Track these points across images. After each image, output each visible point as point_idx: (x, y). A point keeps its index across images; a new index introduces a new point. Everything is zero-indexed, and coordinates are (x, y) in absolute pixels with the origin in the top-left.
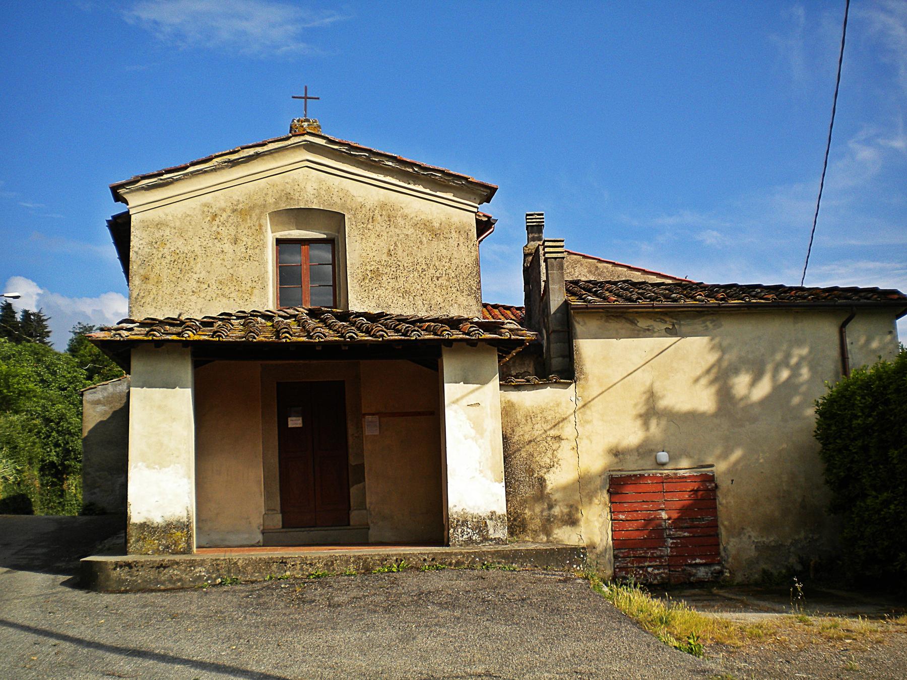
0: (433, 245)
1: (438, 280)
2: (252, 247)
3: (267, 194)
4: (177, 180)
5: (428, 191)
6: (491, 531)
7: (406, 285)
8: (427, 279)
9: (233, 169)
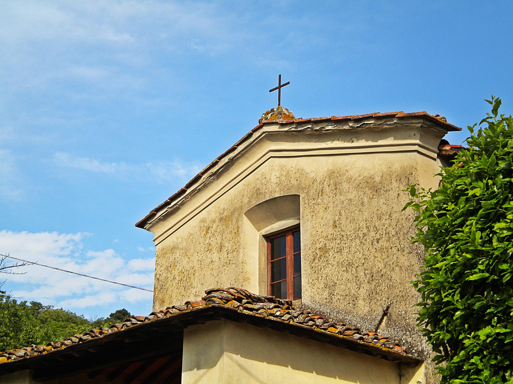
0: (373, 203)
1: (378, 242)
2: (231, 251)
4: (183, 204)
7: (349, 256)
8: (368, 245)
9: (219, 180)
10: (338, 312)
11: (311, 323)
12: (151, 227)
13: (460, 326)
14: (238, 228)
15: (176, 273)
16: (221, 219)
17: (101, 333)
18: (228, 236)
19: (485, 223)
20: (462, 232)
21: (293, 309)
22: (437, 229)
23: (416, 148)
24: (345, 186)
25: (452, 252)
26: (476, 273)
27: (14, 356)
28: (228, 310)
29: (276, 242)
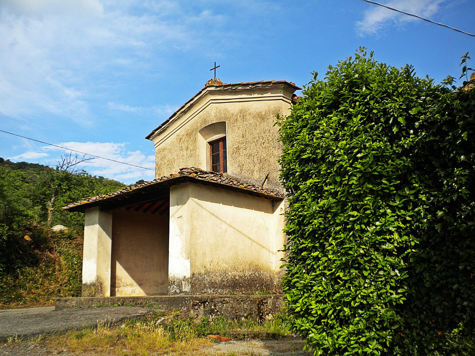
3: (198, 123)
4: (168, 127)
5: (260, 96)
6: (183, 288)
7: (250, 151)
8: (259, 146)
10: (244, 178)
11: (231, 183)
12: (152, 139)
13: (298, 179)
14: (195, 138)
15: (166, 161)
16: (187, 135)
17: (131, 189)
18: (191, 143)
19: (310, 131)
20: (300, 135)
21: (223, 177)
22: (289, 135)
23: (281, 98)
24: (248, 117)
25: (295, 145)
26: (306, 154)
27: (91, 200)
28: (191, 177)
29: (215, 145)
